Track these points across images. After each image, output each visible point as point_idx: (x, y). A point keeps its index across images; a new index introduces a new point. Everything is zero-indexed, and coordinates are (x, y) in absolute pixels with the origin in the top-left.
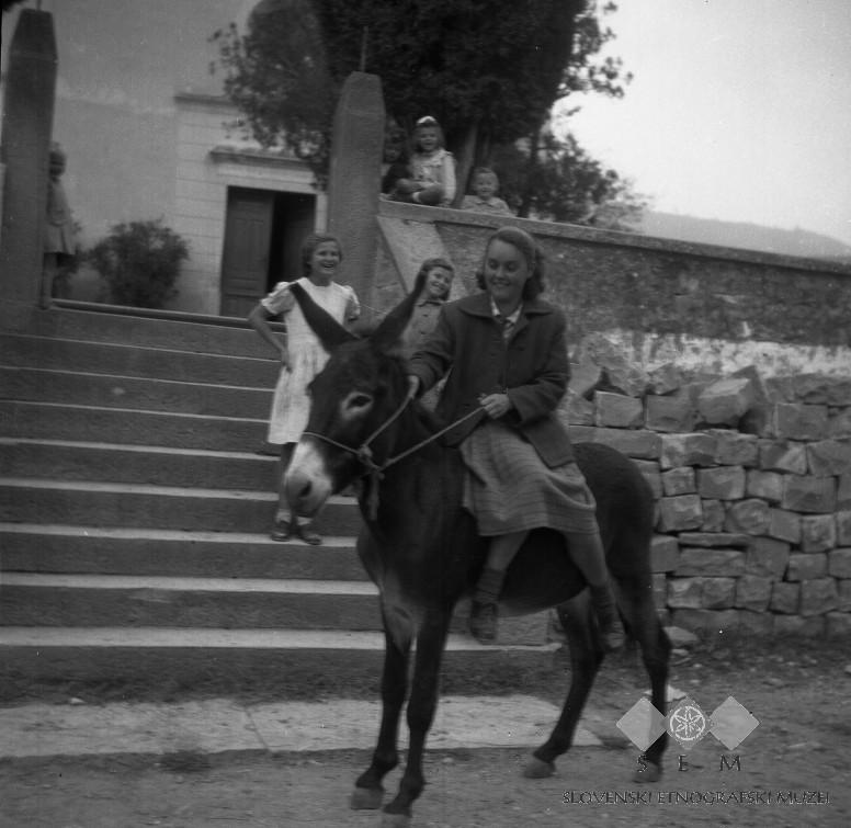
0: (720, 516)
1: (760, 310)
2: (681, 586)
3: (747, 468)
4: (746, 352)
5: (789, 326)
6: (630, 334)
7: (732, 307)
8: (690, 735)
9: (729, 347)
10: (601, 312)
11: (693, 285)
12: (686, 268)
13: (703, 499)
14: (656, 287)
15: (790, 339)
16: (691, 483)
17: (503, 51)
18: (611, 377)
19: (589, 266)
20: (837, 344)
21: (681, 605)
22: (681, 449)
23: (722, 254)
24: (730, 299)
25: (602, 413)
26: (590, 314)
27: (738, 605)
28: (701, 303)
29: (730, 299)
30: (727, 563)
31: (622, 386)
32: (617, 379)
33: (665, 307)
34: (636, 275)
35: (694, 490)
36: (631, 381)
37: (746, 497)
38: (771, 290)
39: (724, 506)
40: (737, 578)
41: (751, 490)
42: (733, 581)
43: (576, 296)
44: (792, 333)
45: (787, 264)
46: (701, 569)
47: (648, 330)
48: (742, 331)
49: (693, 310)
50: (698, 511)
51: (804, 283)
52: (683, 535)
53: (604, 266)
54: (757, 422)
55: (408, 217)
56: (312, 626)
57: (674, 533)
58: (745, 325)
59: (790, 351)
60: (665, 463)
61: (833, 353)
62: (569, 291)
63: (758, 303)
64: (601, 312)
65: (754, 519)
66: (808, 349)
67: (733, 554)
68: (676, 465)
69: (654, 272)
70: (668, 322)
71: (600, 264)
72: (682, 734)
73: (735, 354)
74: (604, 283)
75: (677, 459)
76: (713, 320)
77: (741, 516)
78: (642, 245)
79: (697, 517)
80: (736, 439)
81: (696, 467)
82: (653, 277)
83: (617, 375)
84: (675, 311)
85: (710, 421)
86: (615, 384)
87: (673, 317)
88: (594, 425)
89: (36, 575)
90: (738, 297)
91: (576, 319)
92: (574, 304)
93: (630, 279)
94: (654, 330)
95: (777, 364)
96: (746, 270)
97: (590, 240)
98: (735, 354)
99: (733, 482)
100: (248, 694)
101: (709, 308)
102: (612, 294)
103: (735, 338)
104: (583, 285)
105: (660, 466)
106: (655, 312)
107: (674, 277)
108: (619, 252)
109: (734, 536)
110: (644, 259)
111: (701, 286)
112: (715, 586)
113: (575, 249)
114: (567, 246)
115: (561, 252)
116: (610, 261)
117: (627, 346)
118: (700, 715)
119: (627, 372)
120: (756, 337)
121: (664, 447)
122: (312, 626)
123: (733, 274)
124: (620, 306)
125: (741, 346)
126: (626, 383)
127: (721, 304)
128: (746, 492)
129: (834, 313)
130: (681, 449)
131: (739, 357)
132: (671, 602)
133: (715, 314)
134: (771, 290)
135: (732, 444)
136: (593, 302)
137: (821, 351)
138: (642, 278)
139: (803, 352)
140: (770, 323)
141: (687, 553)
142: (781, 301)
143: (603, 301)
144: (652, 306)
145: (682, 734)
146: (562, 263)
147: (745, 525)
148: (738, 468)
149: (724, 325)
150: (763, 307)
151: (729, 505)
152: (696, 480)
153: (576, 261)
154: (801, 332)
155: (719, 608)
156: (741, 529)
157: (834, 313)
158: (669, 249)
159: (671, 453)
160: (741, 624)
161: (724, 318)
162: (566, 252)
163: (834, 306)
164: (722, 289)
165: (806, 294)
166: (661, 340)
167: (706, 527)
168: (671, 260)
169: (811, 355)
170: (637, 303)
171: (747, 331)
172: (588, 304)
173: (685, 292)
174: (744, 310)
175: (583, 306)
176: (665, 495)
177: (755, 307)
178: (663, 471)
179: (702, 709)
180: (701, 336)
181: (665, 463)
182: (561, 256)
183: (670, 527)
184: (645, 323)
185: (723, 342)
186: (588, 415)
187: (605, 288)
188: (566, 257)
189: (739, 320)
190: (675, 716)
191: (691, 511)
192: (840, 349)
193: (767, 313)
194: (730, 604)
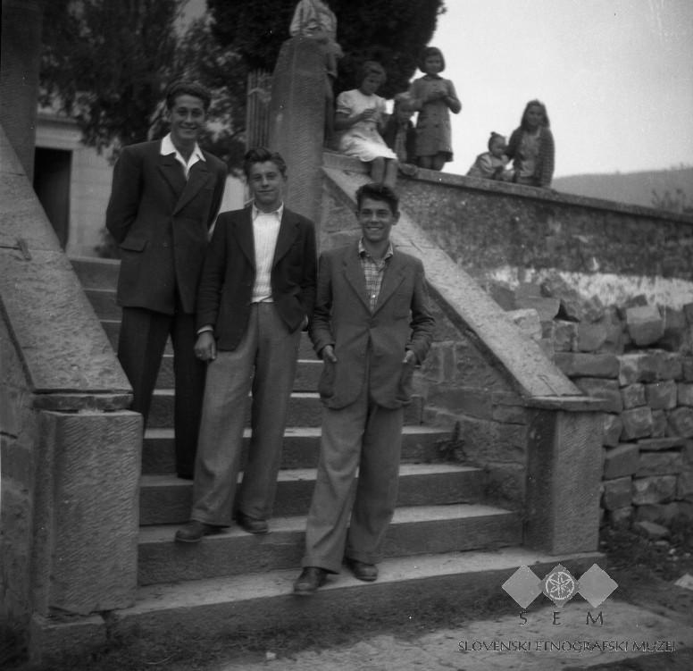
0: (665, 424)
1: (604, 248)
2: (642, 486)
3: (677, 381)
4: (596, 282)
5: (623, 260)
6: (516, 270)
7: (585, 245)
8: (562, 595)
9: (584, 279)
10: (494, 251)
11: (557, 228)
12: (553, 214)
13: (652, 410)
14: (533, 229)
15: (625, 271)
16: (643, 396)
17: (392, 24)
18: (566, 307)
19: (482, 212)
20: (655, 274)
21: (644, 502)
22: (635, 368)
23: (578, 202)
24: (583, 239)
25: (578, 340)
26: (486, 253)
27: (680, 498)
28: (564, 242)
29: (583, 239)
30: (671, 464)
31: (576, 316)
32: (572, 310)
33: (540, 246)
34: (517, 219)
35: (645, 403)
36: (584, 311)
37: (679, 406)
38: (611, 232)
39: (666, 415)
40: (677, 475)
41: (682, 401)
42: (674, 478)
43: (475, 238)
44: (626, 266)
45: (622, 209)
46: (653, 470)
47: (528, 266)
48: (592, 265)
49: (558, 248)
50: (651, 421)
51: (632, 225)
52: (641, 442)
53: (495, 211)
54: (673, 343)
55: (348, 168)
56: (409, 553)
57: (634, 441)
58: (594, 260)
59: (624, 280)
60: (623, 380)
61: (653, 282)
62: (470, 233)
63: (602, 242)
64: (494, 251)
65: (686, 424)
66: (636, 279)
67: (674, 455)
68: (631, 382)
69: (530, 217)
70: (542, 260)
71: (492, 210)
72: (555, 594)
73: (589, 284)
74: (495, 226)
75: (632, 376)
76: (572, 257)
77: (678, 422)
78: (522, 194)
79: (650, 426)
80: (669, 358)
81: (644, 382)
82: (529, 221)
83: (572, 306)
84: (546, 250)
85: (638, 342)
86: (570, 314)
87: (545, 255)
88: (571, 351)
89: (153, 528)
90: (588, 237)
91: (478, 257)
92: (474, 244)
93: (513, 223)
94: (533, 266)
95: (617, 292)
96: (594, 214)
97: (485, 189)
98: (589, 284)
99: (667, 392)
100: (402, 628)
101: (569, 247)
102: (501, 236)
103: (588, 272)
104: (481, 228)
105: (619, 383)
106: (532, 250)
107: (544, 221)
108: (505, 200)
109: (674, 440)
110: (523, 205)
111: (563, 229)
112: (664, 483)
113: (472, 196)
114: (467, 194)
115: (464, 200)
116: (498, 207)
117: (514, 280)
118: (570, 579)
119: (581, 303)
120: (602, 270)
121: (621, 367)
122: (409, 553)
123: (584, 218)
124: (508, 246)
125: (592, 278)
126: (580, 313)
127: (577, 243)
128: (677, 402)
129: (653, 249)
130: (635, 368)
131: (592, 288)
132: (635, 500)
133: (574, 251)
134: (611, 232)
135: (667, 361)
136: (488, 242)
137: (645, 280)
138: (521, 221)
139: (633, 282)
140: (611, 259)
141: (644, 457)
142: (619, 241)
143: (495, 242)
144: (530, 245)
145: (555, 594)
146: (464, 209)
147: (681, 429)
148: (672, 382)
149: (580, 261)
150: (606, 246)
151: (668, 414)
152: (646, 394)
153: (474, 208)
154: (632, 265)
155: (665, 502)
156: (678, 433)
157: (653, 249)
158: (541, 197)
159: (627, 372)
160: (682, 515)
161: (580, 255)
162: (467, 200)
163: (652, 244)
164: (578, 230)
165: (634, 234)
166: (538, 275)
167: (655, 434)
168: (542, 206)
169: (639, 284)
170: (519, 242)
171: (596, 266)
172: (484, 245)
173: (552, 233)
174: (593, 247)
175: (481, 246)
176: (624, 408)
177: (600, 246)
178: (621, 387)
179: (572, 574)
180: (564, 270)
181: (623, 380)
182: (464, 203)
183: (632, 436)
184: (526, 260)
185: (581, 275)
186: (566, 342)
187: (496, 231)
188: (467, 204)
189: (590, 256)
190: (550, 579)
191: (646, 421)
192: (657, 278)
193: (609, 250)
194: (674, 497)
